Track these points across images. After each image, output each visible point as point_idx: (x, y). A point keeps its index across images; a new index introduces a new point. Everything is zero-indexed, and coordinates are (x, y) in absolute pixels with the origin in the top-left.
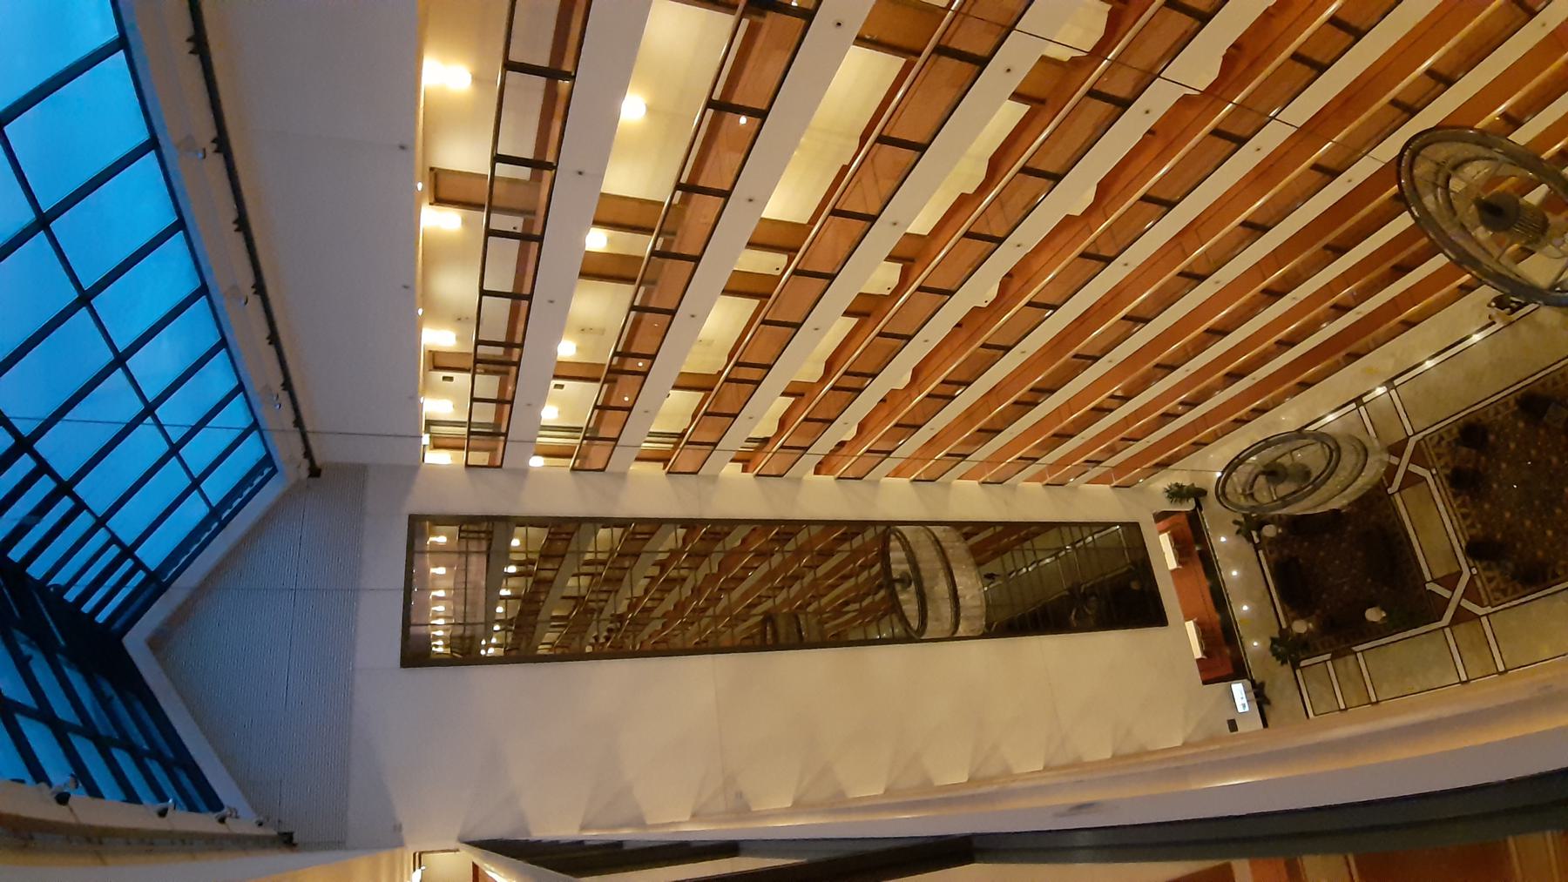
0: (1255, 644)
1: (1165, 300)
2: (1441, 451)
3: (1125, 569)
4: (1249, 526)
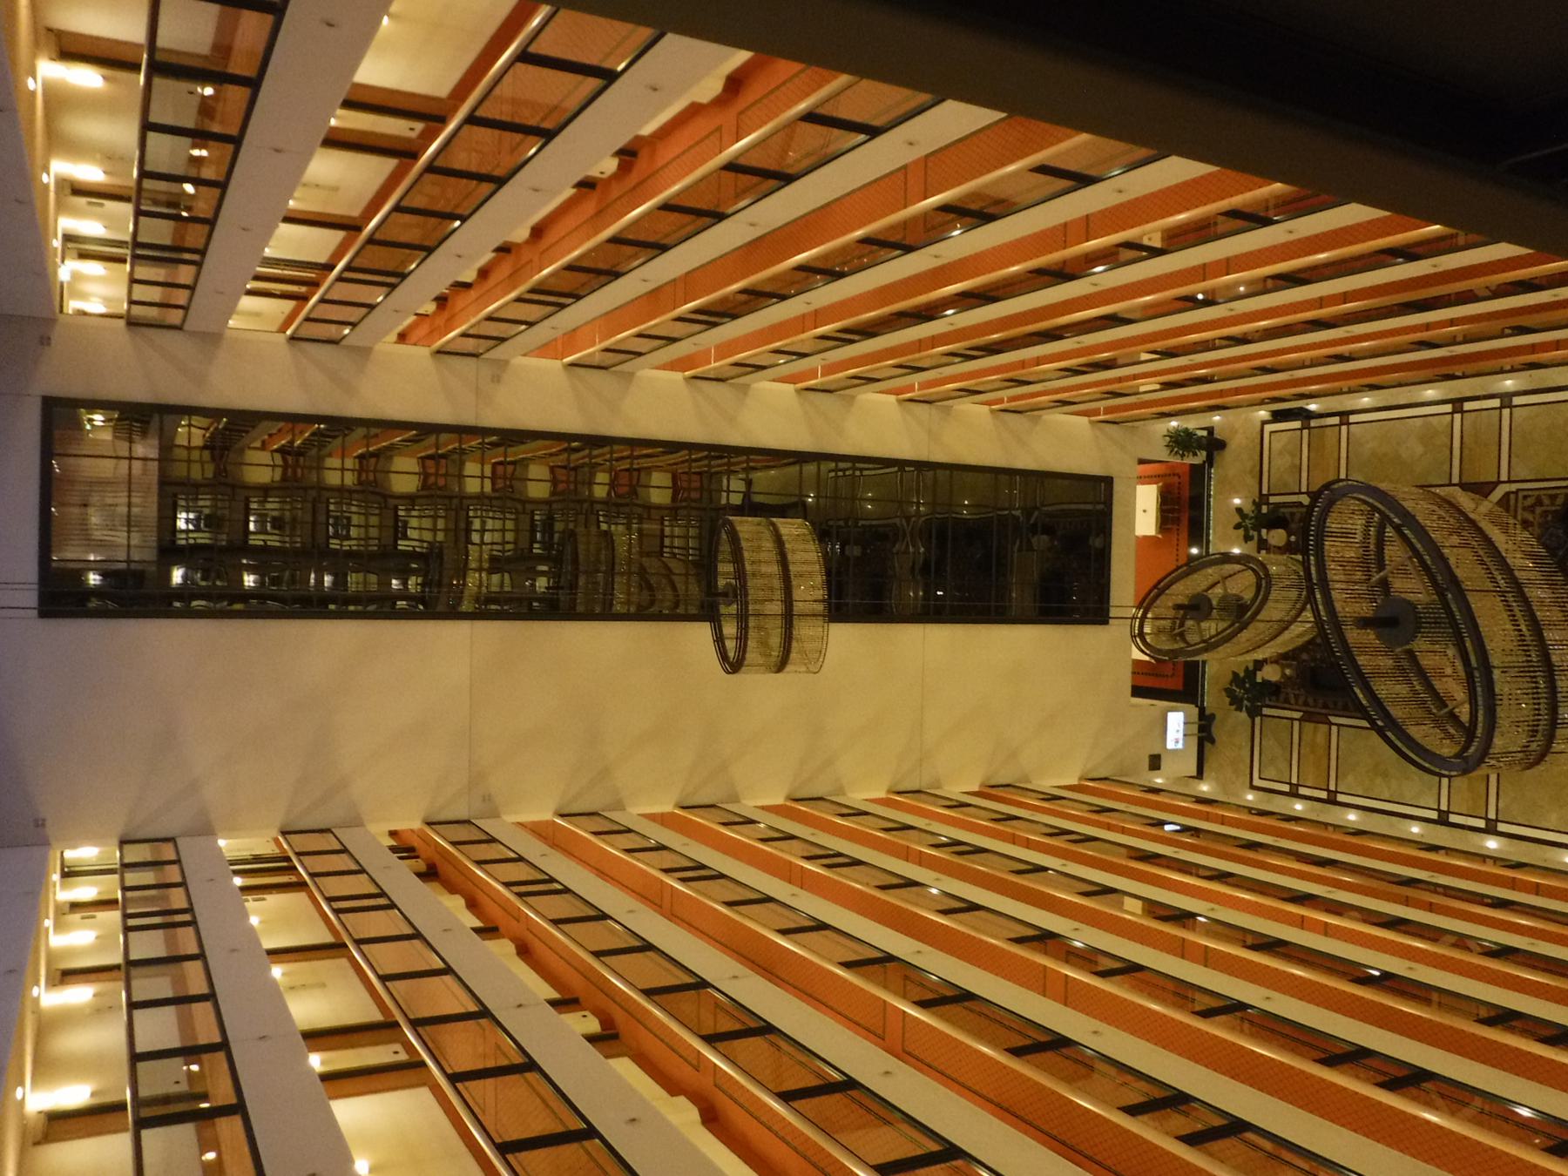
2: (1530, 517)
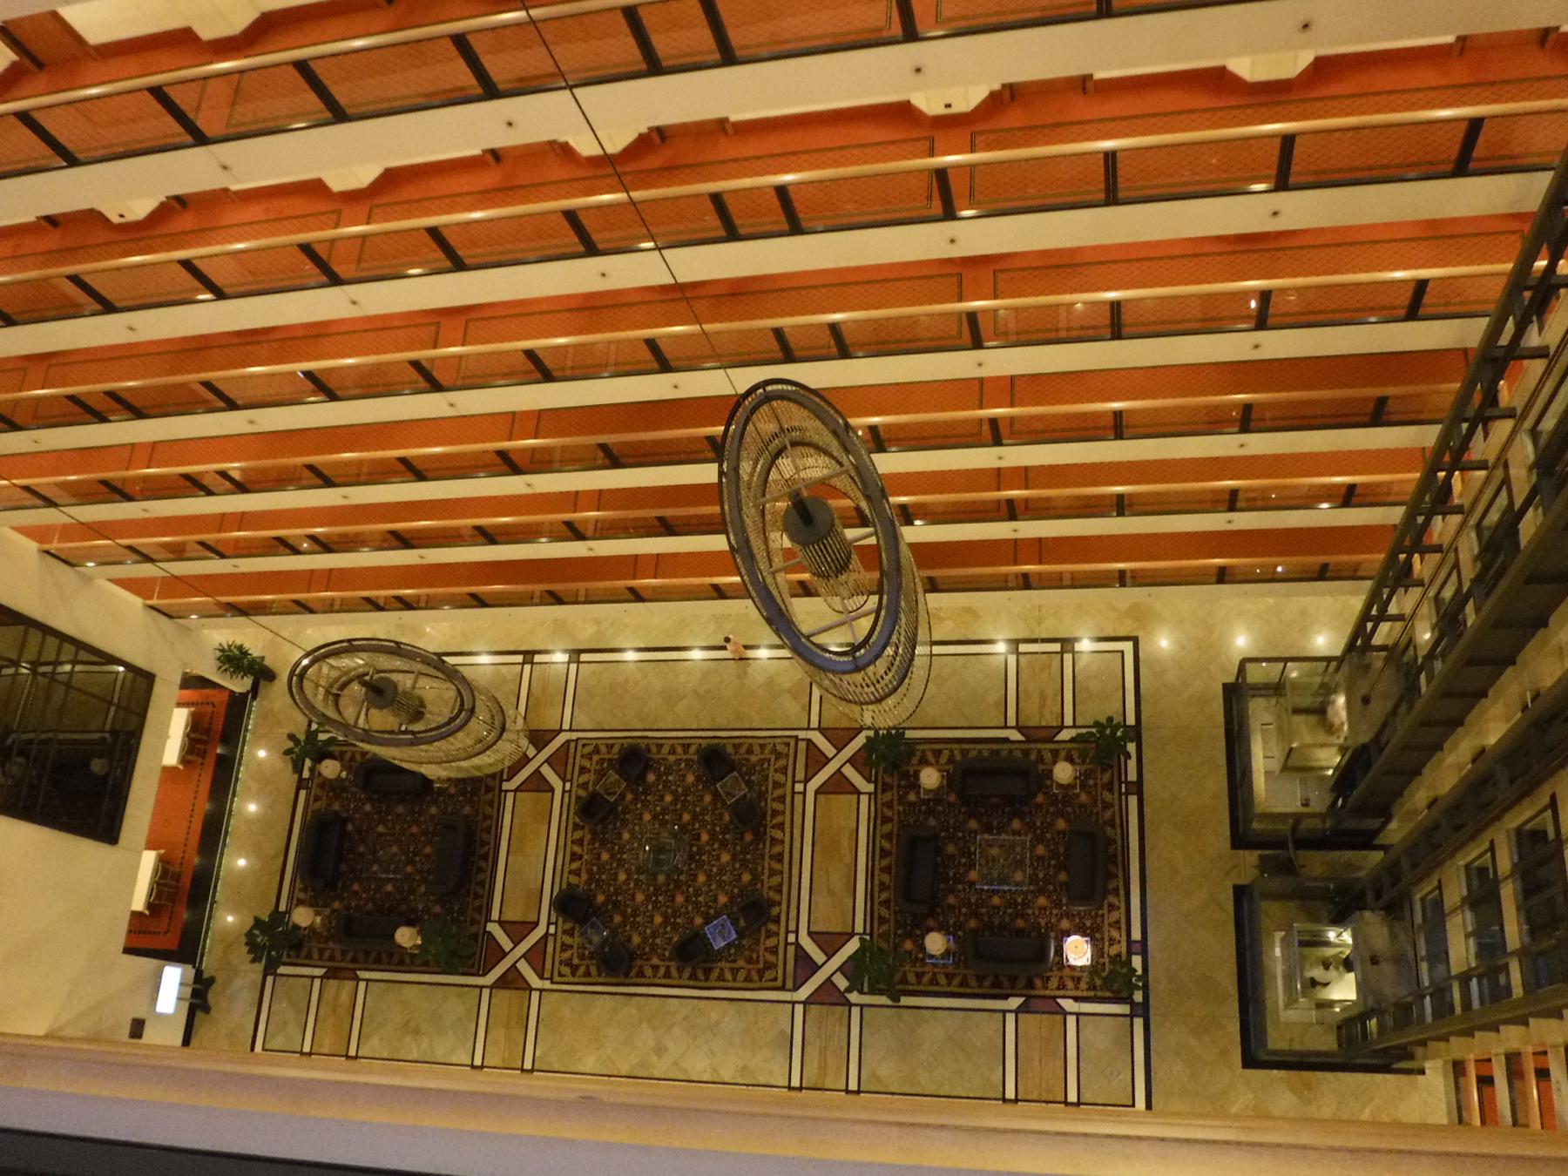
0: (230, 919)
1: (373, 385)
3: (96, 736)
4: (304, 751)
